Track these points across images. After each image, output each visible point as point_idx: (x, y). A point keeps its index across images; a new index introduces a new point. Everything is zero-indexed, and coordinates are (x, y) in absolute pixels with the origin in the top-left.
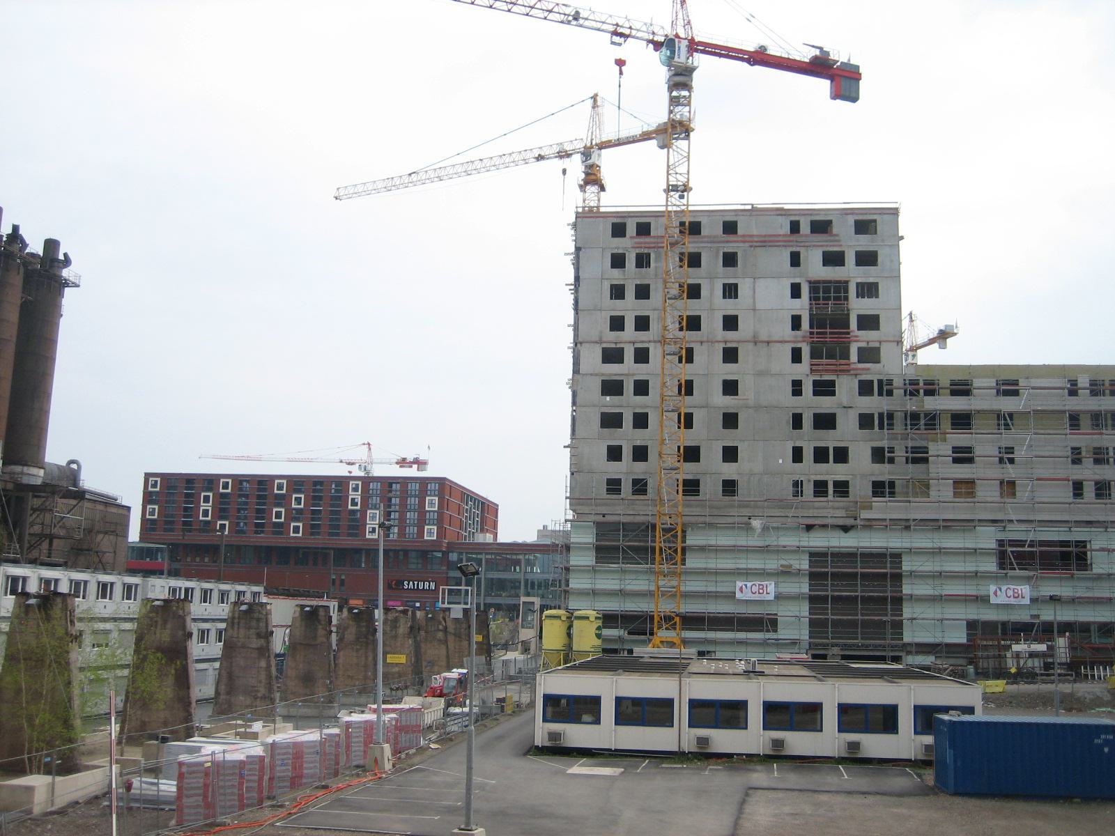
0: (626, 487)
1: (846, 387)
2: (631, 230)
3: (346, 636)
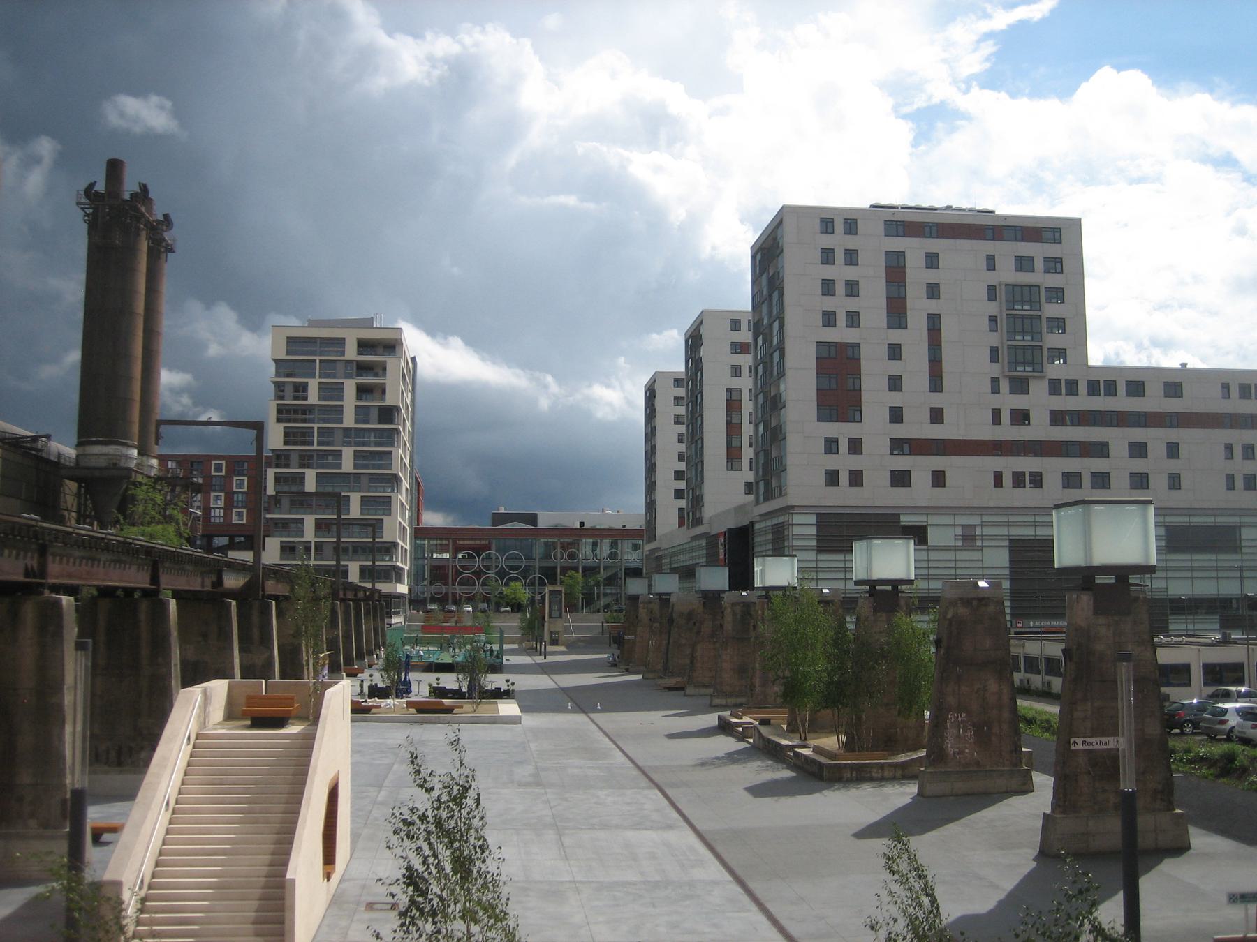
0: (844, 478)
1: (1039, 389)
2: (839, 227)
3: (702, 630)
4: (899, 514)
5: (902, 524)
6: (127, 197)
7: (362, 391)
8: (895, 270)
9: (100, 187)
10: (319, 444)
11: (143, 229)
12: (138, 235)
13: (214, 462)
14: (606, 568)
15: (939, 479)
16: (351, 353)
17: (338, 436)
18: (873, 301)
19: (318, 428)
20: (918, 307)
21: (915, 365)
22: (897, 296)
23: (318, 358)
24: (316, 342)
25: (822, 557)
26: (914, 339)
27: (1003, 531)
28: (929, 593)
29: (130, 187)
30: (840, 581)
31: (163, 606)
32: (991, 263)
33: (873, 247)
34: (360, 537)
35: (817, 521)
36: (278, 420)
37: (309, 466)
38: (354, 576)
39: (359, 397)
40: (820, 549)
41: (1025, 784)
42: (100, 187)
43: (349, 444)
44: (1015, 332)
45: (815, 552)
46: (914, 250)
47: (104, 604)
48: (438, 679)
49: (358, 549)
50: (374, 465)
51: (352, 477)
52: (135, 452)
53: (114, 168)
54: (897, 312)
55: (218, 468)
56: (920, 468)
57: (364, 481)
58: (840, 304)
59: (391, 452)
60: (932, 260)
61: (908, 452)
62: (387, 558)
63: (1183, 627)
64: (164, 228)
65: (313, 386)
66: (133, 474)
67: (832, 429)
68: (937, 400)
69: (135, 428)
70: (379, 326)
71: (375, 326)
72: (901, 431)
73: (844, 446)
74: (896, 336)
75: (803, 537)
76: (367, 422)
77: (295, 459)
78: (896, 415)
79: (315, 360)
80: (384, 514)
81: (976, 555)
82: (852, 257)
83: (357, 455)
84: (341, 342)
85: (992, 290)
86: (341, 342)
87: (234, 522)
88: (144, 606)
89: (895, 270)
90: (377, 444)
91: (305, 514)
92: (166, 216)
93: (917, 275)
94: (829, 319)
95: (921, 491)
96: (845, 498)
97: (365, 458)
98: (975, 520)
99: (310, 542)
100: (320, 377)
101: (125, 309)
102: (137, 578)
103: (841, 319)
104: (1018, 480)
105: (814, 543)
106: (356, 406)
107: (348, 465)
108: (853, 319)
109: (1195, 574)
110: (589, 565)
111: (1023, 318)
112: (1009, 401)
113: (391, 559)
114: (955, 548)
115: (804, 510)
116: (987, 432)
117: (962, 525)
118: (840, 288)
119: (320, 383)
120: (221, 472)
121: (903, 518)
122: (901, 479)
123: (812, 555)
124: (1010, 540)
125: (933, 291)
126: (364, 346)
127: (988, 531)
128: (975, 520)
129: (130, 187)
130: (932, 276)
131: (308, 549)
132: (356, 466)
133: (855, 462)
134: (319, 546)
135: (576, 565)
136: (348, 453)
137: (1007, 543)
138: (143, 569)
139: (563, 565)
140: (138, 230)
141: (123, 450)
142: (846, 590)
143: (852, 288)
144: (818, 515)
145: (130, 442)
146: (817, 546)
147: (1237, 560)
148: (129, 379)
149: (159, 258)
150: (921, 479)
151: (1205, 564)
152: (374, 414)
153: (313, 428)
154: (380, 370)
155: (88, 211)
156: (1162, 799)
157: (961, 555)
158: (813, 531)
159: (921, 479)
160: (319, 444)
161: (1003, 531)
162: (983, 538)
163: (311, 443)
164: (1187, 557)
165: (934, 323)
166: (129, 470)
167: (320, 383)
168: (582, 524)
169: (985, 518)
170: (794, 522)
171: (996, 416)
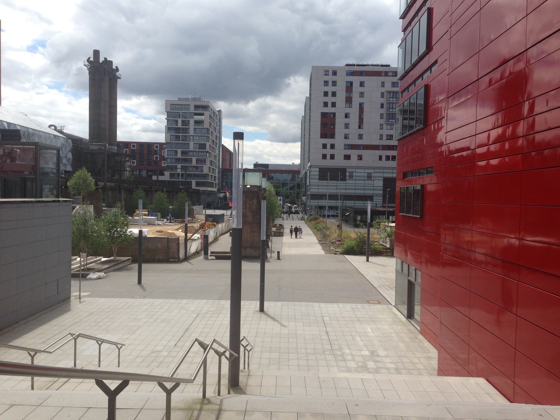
0: (328, 157)
6: (101, 62)
8: (349, 87)
9: (92, 59)
13: (132, 144)
15: (360, 158)
16: (192, 109)
20: (356, 100)
21: (354, 120)
22: (349, 96)
25: (320, 181)
26: (354, 111)
27: (381, 175)
29: (102, 59)
32: (383, 85)
33: (342, 80)
35: (319, 170)
38: (194, 186)
40: (320, 179)
42: (92, 59)
44: (390, 108)
45: (318, 180)
46: (356, 80)
49: (195, 176)
54: (349, 100)
55: (157, 147)
56: (354, 154)
58: (330, 99)
60: (362, 84)
61: (381, 149)
63: (356, 204)
67: (325, 141)
68: (361, 131)
72: (348, 142)
73: (329, 146)
74: (348, 110)
75: (315, 175)
78: (346, 137)
80: (178, 164)
81: (371, 182)
82: (334, 83)
85: (382, 94)
87: (162, 166)
89: (349, 87)
92: (117, 67)
93: (356, 88)
94: (326, 105)
95: (354, 161)
96: (328, 163)
98: (372, 171)
100: (182, 118)
103: (330, 105)
104: (388, 158)
105: (318, 177)
108: (334, 105)
111: (396, 104)
112: (386, 132)
114: (365, 180)
116: (376, 142)
117: (367, 173)
118: (330, 94)
120: (133, 147)
122: (347, 157)
123: (317, 181)
124: (384, 178)
125: (362, 95)
126: (196, 107)
127: (376, 175)
128: (372, 171)
129: (102, 59)
130: (361, 89)
133: (332, 152)
134: (182, 175)
137: (382, 179)
143: (334, 94)
144: (319, 168)
147: (335, 183)
150: (354, 158)
151: (324, 184)
155: (89, 67)
157: (366, 182)
158: (318, 173)
159: (354, 158)
161: (381, 175)
162: (374, 177)
165: (361, 106)
169: (376, 170)
171: (381, 137)
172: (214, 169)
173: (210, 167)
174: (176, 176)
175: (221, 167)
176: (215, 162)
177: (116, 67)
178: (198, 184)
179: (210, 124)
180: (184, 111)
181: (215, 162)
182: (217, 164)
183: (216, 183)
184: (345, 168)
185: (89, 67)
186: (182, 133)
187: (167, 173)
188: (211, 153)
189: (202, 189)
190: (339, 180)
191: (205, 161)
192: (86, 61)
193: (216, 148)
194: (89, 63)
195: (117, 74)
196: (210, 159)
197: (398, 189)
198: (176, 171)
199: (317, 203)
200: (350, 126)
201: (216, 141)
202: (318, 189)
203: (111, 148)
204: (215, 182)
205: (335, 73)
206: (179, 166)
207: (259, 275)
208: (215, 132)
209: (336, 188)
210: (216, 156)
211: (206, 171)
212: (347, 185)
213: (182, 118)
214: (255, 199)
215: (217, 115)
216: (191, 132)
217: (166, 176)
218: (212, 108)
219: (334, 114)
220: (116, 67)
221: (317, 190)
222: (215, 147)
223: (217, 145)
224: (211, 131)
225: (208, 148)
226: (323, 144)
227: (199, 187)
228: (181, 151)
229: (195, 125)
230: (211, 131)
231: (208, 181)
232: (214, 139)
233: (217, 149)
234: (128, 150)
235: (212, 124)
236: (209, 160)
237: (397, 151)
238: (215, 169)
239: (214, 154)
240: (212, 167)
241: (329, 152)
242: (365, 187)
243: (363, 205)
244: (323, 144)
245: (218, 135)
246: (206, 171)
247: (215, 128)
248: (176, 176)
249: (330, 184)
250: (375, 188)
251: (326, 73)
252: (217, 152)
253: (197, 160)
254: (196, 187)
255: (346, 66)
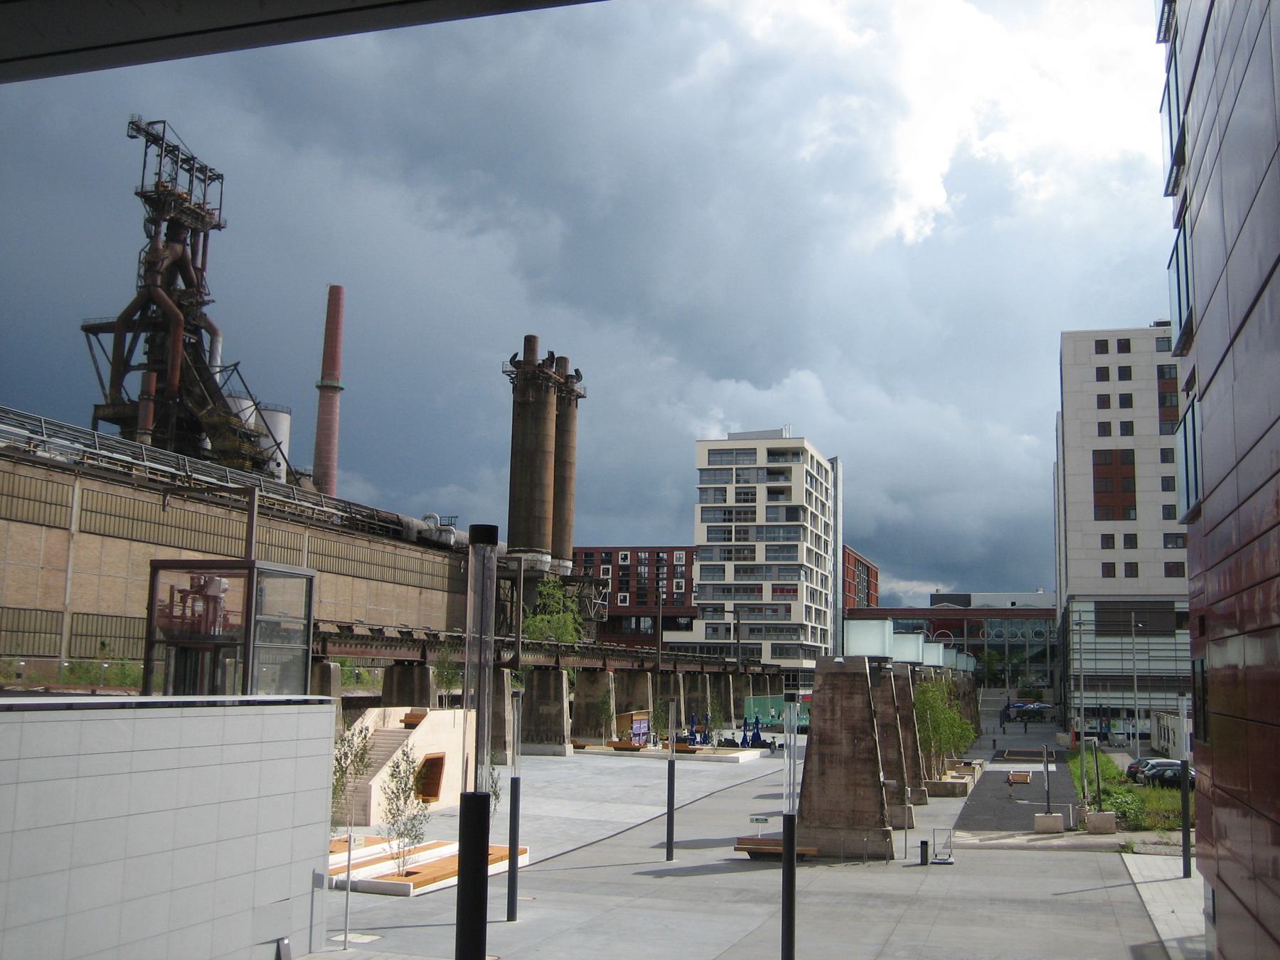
0: (1120, 570)
2: (1113, 346)
4: (1173, 602)
5: (1176, 610)
7: (773, 493)
9: (520, 357)
10: (736, 540)
11: (552, 387)
12: (547, 391)
14: (1031, 646)
16: (762, 460)
17: (752, 533)
18: (1146, 411)
19: (736, 526)
23: (734, 467)
24: (732, 453)
28: (1096, 672)
29: (541, 355)
30: (1145, 662)
31: (427, 670)
33: (1145, 362)
34: (772, 620)
35: (1095, 609)
36: (702, 520)
37: (730, 559)
39: (769, 499)
40: (1099, 633)
41: (920, 799)
42: (520, 357)
43: (762, 540)
45: (1093, 636)
47: (397, 669)
48: (733, 734)
50: (783, 557)
51: (764, 569)
52: (549, 558)
53: (530, 342)
57: (775, 570)
59: (797, 546)
62: (795, 637)
63: (1153, 702)
64: (575, 381)
65: (731, 490)
66: (545, 574)
67: (1108, 527)
69: (549, 539)
70: (788, 436)
71: (784, 436)
73: (1119, 541)
76: (776, 520)
77: (716, 552)
79: (732, 469)
82: (1125, 373)
83: (768, 549)
84: (752, 452)
86: (752, 452)
88: (416, 671)
90: (784, 540)
91: (726, 600)
92: (577, 371)
94: (1104, 429)
96: (1121, 587)
97: (776, 551)
99: (730, 624)
101: (540, 449)
102: (414, 656)
103: (1116, 429)
105: (1093, 627)
106: (767, 506)
107: (760, 558)
108: (1127, 428)
109: (1099, 656)
110: (1015, 643)
113: (798, 639)
115: (1085, 597)
119: (736, 488)
121: (1177, 605)
126: (773, 454)
129: (541, 355)
131: (728, 630)
132: (767, 559)
135: (1003, 643)
136: (761, 547)
138: (414, 650)
139: (990, 643)
140: (548, 388)
141: (539, 556)
142: (1149, 669)
143: (1126, 401)
145: (544, 550)
146: (1096, 631)
148: (543, 502)
149: (570, 405)
152: (783, 513)
153: (731, 526)
154: (784, 473)
155: (513, 376)
156: (897, 798)
158: (1092, 617)
160: (736, 540)
163: (730, 540)
164: (1118, 640)
166: (542, 572)
167: (736, 488)
168: (1013, 604)
170: (1074, 610)
172: (820, 610)
173: (810, 607)
174: (722, 630)
175: (840, 605)
176: (824, 591)
177: (575, 370)
178: (778, 651)
179: (809, 494)
180: (743, 464)
181: (824, 591)
182: (830, 599)
183: (826, 649)
184: (1170, 599)
185: (513, 376)
186: (737, 520)
187: (699, 625)
188: (812, 570)
189: (786, 663)
190: (1133, 633)
191: (796, 591)
192: (509, 363)
193: (824, 555)
194: (515, 367)
195: (578, 387)
196: (810, 585)
197: (505, 669)
198: (788, 617)
199: (1147, 702)
200: (1158, 484)
201: (827, 539)
202: (1122, 660)
203: (559, 565)
204: (824, 646)
205: (1124, 346)
206: (729, 606)
207: (778, 908)
208: (823, 514)
209: (1146, 657)
210: (826, 577)
211: (798, 616)
212: (1179, 647)
213: (738, 482)
214: (858, 694)
215: (827, 471)
216: (761, 519)
217: (698, 633)
218: (814, 455)
219: (1130, 453)
220: (575, 370)
221: (1118, 665)
222: (822, 553)
223: (829, 547)
224: (812, 513)
225: (803, 558)
226: (1103, 536)
227: (780, 658)
228: (735, 565)
229: (769, 499)
230: (812, 513)
231: (805, 642)
232: (819, 533)
233: (829, 557)
234: (610, 567)
235: (815, 494)
236: (807, 586)
237: (1185, 550)
238: (825, 612)
239: (820, 571)
240: (814, 606)
241: (1120, 555)
242: (1178, 652)
243: (1120, 702)
244: (1103, 536)
245: (831, 523)
246: (798, 616)
247: (823, 505)
248: (722, 630)
249: (1137, 647)
250: (1119, 656)
251: (1102, 347)
252: (830, 566)
253: (775, 589)
254: (772, 658)
255: (1157, 326)
